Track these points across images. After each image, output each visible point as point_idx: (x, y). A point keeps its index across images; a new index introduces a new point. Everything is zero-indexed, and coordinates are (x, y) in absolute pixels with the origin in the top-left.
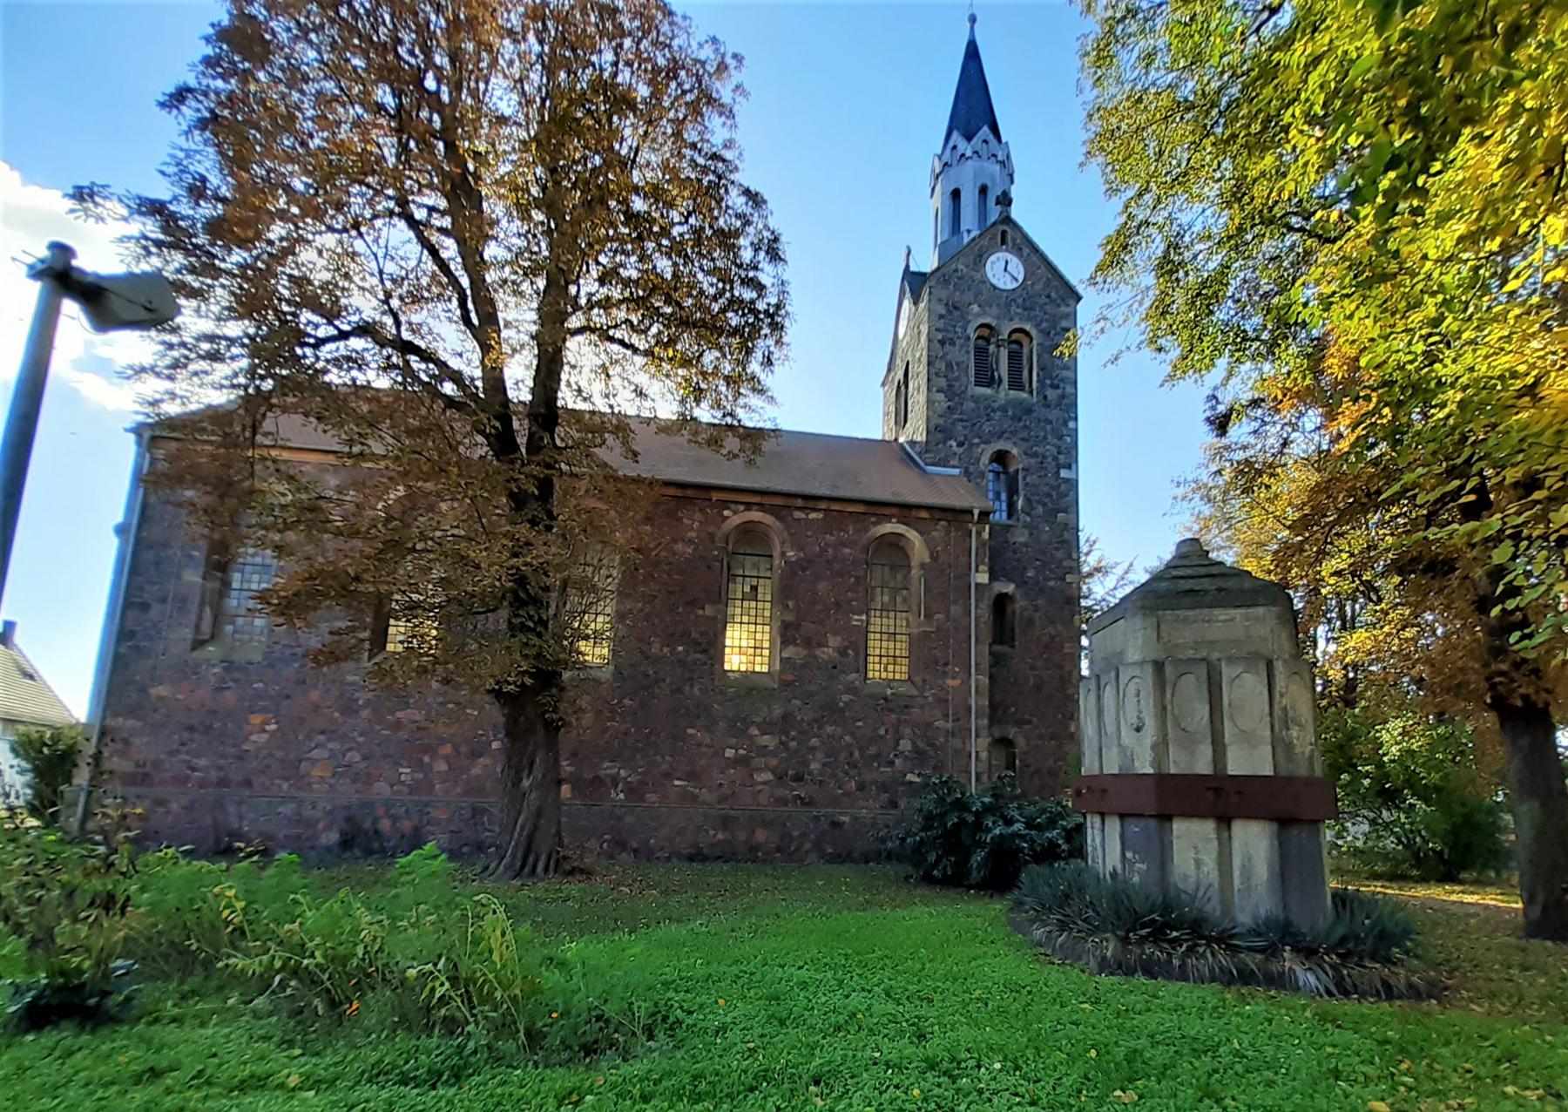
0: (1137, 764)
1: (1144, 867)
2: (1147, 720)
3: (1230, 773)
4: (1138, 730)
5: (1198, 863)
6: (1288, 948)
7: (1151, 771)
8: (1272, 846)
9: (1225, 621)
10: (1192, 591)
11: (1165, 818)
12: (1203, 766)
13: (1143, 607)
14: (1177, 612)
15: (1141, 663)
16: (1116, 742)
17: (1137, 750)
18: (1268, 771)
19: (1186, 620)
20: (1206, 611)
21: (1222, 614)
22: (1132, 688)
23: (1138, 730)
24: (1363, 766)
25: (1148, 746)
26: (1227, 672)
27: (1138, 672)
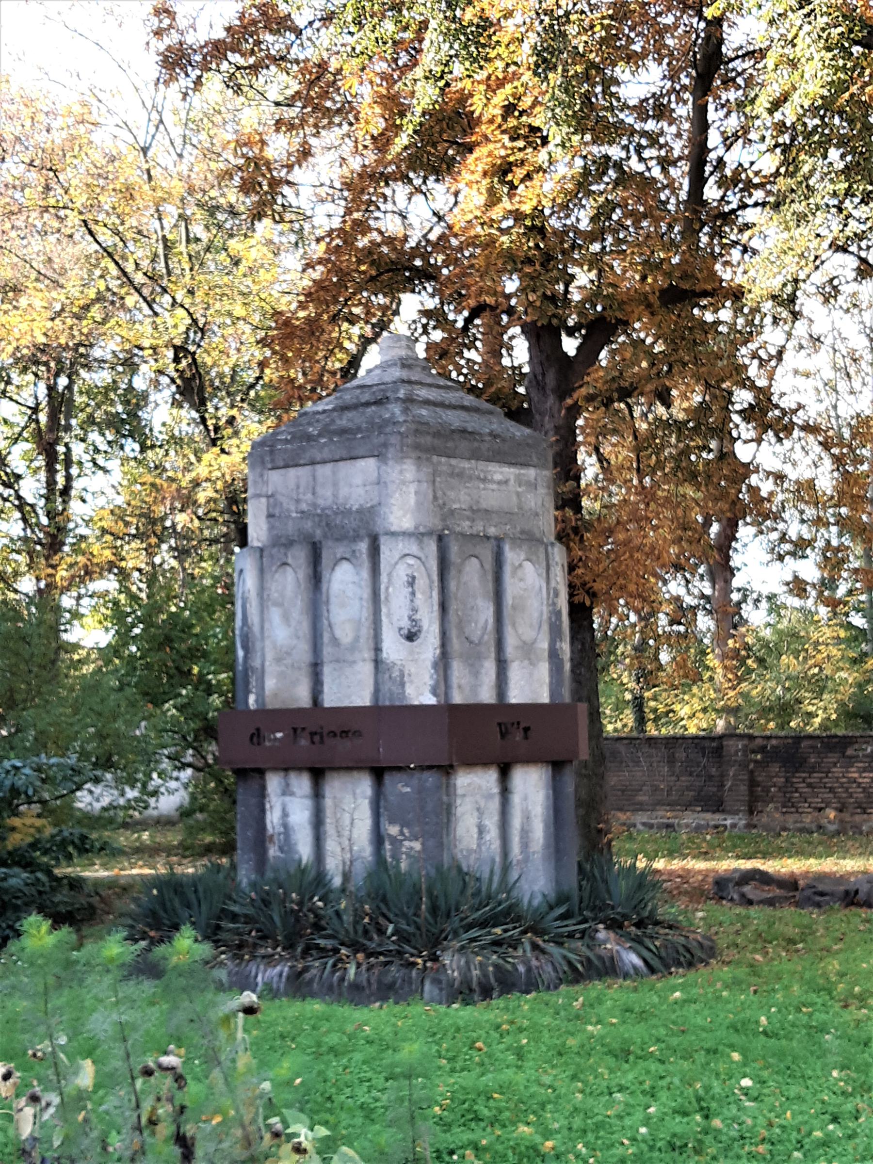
0: (410, 690)
1: (417, 846)
2: (425, 624)
3: (513, 701)
4: (411, 637)
5: (481, 830)
6: (601, 926)
7: (430, 700)
8: (547, 797)
9: (499, 483)
10: (464, 431)
11: (447, 770)
12: (487, 695)
13: (417, 447)
14: (453, 461)
15: (417, 535)
16: (368, 654)
17: (410, 668)
18: (545, 698)
19: (460, 475)
20: (482, 465)
21: (500, 472)
22: (402, 573)
23: (411, 637)
24: (214, 673)
25: (429, 664)
26: (511, 556)
27: (414, 549)
